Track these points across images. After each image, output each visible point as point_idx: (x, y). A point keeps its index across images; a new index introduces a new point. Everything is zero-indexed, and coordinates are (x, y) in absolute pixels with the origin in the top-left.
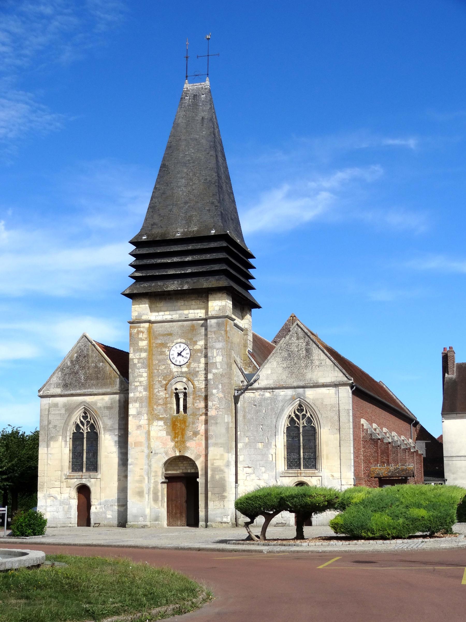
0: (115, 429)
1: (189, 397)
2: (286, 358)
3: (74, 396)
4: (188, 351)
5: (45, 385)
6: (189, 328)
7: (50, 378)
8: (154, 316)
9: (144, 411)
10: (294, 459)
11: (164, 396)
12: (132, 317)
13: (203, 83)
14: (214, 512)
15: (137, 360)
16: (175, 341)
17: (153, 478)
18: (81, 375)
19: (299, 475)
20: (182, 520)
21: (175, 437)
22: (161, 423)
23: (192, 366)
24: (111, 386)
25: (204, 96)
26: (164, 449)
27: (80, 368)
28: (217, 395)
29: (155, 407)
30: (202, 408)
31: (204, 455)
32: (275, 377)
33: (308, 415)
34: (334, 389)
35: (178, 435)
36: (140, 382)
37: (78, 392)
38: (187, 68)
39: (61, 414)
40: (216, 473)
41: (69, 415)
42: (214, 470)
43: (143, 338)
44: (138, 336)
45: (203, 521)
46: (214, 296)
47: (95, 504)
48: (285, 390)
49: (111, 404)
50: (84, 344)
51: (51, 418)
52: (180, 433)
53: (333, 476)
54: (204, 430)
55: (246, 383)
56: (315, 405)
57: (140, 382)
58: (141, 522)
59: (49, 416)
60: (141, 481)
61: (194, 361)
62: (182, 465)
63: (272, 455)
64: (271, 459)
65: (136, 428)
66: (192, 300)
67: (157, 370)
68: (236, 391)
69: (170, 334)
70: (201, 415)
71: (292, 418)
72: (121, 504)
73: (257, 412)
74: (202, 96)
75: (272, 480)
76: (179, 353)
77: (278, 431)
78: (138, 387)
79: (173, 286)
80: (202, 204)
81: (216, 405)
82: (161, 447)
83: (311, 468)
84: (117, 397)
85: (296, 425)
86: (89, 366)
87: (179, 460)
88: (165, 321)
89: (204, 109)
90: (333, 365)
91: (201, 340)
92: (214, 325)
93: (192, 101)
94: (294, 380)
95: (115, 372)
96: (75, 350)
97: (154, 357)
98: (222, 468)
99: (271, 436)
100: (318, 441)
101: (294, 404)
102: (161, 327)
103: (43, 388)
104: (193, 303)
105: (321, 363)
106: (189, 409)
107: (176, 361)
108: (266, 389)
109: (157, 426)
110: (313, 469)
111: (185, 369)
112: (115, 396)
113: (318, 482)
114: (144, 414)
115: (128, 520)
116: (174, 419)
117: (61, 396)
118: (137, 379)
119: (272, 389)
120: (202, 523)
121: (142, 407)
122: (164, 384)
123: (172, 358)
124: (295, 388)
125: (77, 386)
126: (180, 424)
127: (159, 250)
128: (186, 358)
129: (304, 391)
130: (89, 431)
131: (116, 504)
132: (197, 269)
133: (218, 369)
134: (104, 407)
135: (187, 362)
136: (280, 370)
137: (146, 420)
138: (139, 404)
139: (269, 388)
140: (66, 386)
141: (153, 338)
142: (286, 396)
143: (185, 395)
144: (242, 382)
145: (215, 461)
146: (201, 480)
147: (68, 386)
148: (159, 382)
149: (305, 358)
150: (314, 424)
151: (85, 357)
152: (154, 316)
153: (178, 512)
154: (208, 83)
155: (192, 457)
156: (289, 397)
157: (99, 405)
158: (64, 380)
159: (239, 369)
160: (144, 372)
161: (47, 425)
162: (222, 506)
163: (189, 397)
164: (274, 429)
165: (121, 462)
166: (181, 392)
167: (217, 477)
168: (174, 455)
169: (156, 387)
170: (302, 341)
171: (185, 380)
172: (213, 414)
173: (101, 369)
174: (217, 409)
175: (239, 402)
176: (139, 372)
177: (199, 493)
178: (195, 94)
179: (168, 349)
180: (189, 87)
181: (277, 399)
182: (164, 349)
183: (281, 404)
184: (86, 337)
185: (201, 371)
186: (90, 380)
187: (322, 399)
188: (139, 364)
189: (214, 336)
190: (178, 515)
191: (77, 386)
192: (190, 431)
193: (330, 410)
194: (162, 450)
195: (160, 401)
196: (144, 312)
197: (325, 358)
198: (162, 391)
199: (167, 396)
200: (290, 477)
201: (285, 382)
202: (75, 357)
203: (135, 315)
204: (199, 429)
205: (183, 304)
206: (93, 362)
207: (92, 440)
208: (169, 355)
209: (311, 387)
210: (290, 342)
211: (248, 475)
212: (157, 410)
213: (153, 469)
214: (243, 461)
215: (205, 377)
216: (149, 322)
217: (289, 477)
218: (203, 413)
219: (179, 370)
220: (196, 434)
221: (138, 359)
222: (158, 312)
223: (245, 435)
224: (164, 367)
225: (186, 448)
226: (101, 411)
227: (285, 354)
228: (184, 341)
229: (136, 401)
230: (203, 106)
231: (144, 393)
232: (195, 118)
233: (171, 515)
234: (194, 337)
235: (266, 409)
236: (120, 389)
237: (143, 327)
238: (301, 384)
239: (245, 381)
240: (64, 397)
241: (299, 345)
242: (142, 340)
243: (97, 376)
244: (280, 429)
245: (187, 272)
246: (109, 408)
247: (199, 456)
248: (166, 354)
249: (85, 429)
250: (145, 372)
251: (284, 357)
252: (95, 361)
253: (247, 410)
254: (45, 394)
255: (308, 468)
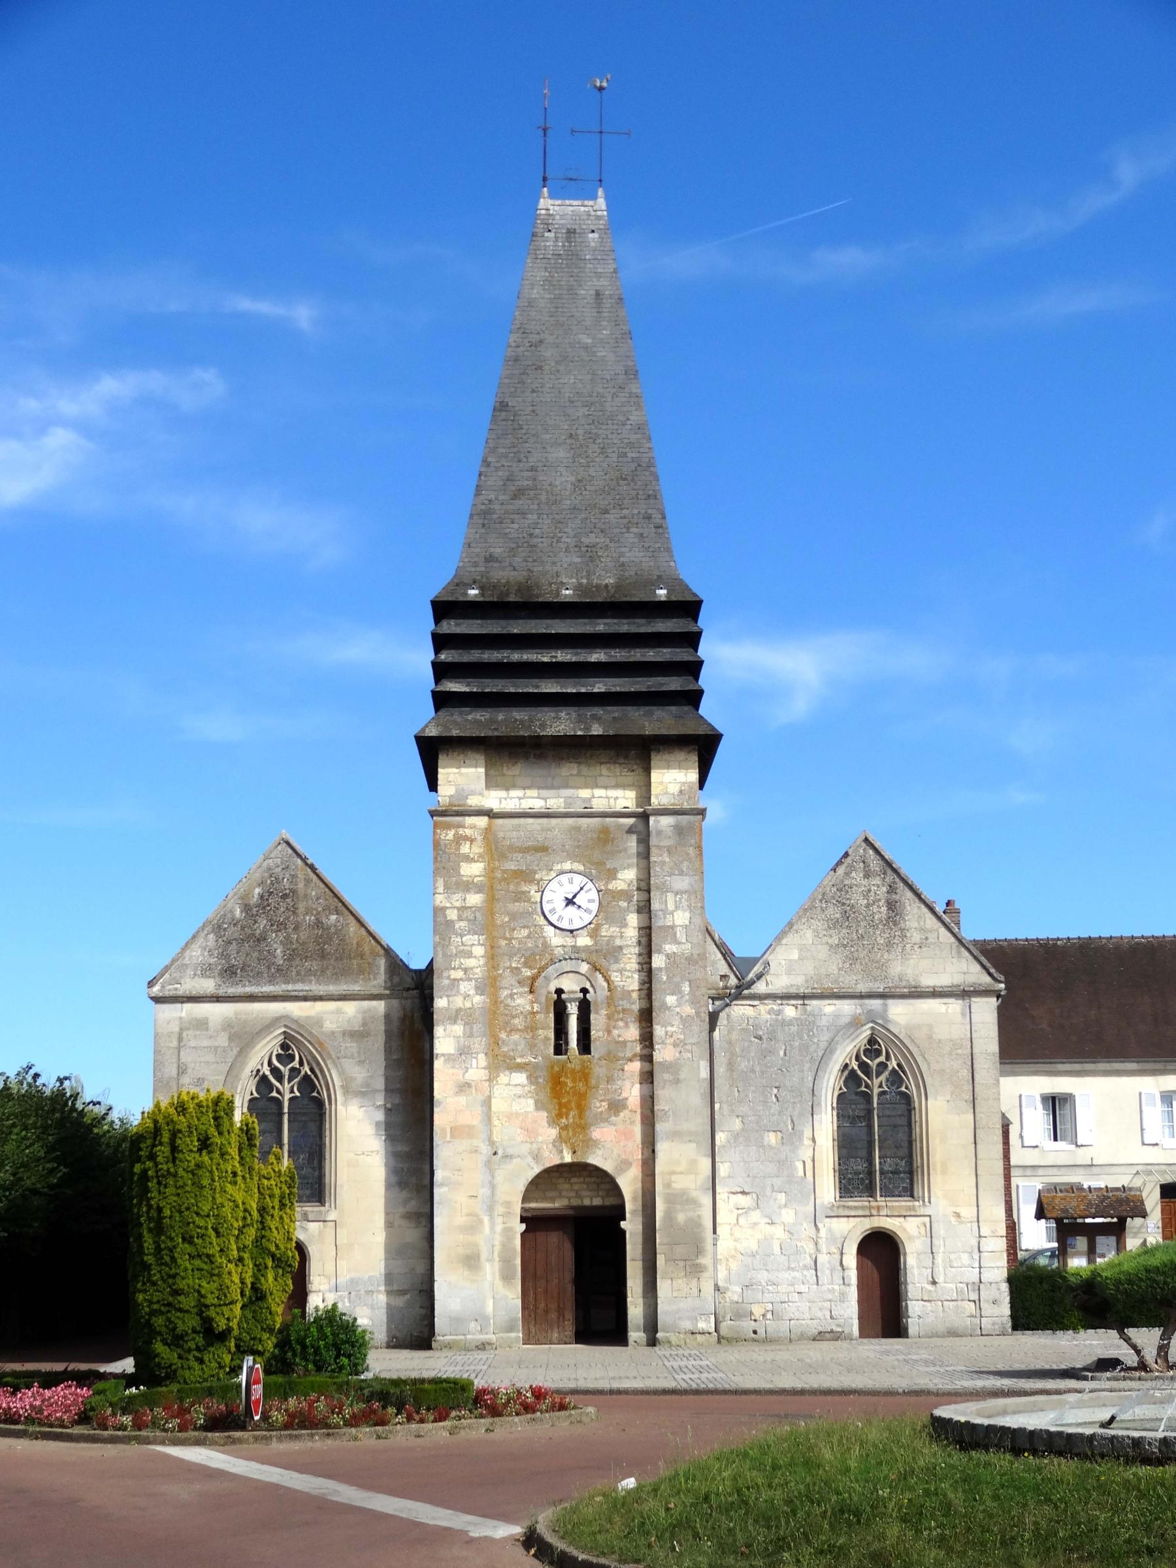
0: (375, 1091)
1: (597, 1013)
2: (837, 921)
3: (253, 1001)
4: (594, 895)
5: (166, 969)
6: (595, 836)
7: (184, 949)
8: (495, 800)
9: (476, 1046)
10: (857, 1173)
11: (528, 1008)
12: (439, 799)
13: (591, 203)
14: (675, 1307)
15: (456, 911)
16: (558, 867)
17: (499, 1220)
18: (275, 946)
19: (874, 1212)
20: (564, 1327)
21: (560, 1116)
22: (520, 1078)
23: (604, 932)
24: (362, 977)
25: (596, 235)
26: (528, 1145)
27: (272, 925)
28: (678, 1010)
29: (503, 1035)
30: (632, 1041)
31: (640, 1163)
32: (809, 968)
33: (893, 1064)
34: (960, 1002)
35: (569, 1110)
36: (466, 970)
37: (267, 989)
38: (545, 157)
39: (216, 1048)
40: (679, 1207)
41: (240, 1052)
42: (671, 1200)
43: (472, 856)
44: (458, 849)
45: (638, 1330)
46: (666, 756)
47: (322, 1288)
48: (834, 1002)
49: (364, 1024)
50: (282, 863)
51: (186, 1057)
52: (573, 1105)
53: (958, 1215)
54: (639, 1098)
55: (733, 981)
56: (913, 1041)
57: (466, 970)
58: (473, 1334)
59: (182, 1053)
60: (473, 1227)
61: (610, 920)
62: (567, 1186)
63: (804, 1162)
64: (801, 1173)
65: (457, 1090)
66: (601, 763)
67: (506, 939)
68: (710, 1001)
69: (543, 849)
70: (631, 1060)
71: (264, 1077)
72: (395, 1287)
73: (764, 1054)
74: (591, 235)
75: (805, 1225)
76: (570, 897)
77: (819, 1104)
78: (461, 982)
79: (561, 723)
80: (618, 516)
81: (675, 1036)
82: (519, 1139)
83: (899, 1196)
84: (380, 1006)
85: (274, 1094)
86: (298, 922)
87: (558, 1174)
88: (529, 813)
89: (599, 270)
90: (957, 943)
91: (629, 866)
92: (669, 831)
93: (564, 246)
94: (860, 977)
95: (373, 941)
96: (257, 876)
97: (498, 906)
98: (694, 1194)
99: (801, 1115)
100: (918, 1130)
101: (857, 1037)
102: (517, 828)
103: (162, 974)
104: (604, 771)
105: (927, 939)
106: (598, 1043)
107: (560, 918)
108: (787, 997)
109: (509, 1084)
110: (906, 1199)
111: (584, 941)
112: (374, 1003)
113: (923, 1230)
114: (477, 1053)
115: (437, 1330)
116: (556, 1069)
117: (217, 999)
118: (457, 962)
119: (804, 997)
120: (636, 1335)
121: (471, 1035)
122: (528, 977)
123: (550, 911)
124: (861, 996)
125: (262, 973)
126: (574, 1081)
127: (517, 627)
128: (587, 911)
129: (885, 1005)
130: (298, 1094)
131: (382, 1288)
132: (619, 686)
133: (680, 943)
134: (344, 1033)
135: (590, 923)
136: (822, 952)
137: (484, 1068)
138: (462, 1027)
139: (796, 997)
140: (229, 973)
141: (496, 857)
142: (837, 1016)
143: (585, 1008)
144: (723, 977)
145: (674, 1178)
146: (631, 1226)
147: (236, 973)
148: (512, 971)
149: (885, 925)
150: (907, 1088)
151: (285, 896)
152: (495, 800)
153: (553, 1306)
154: (601, 203)
155: (608, 1167)
156: (846, 1020)
157: (329, 1026)
158: (224, 955)
159: (716, 944)
160: (476, 943)
161: (175, 1076)
162: (695, 1291)
163: (597, 1013)
164: (808, 1096)
165: (394, 1179)
166: (574, 1000)
167: (681, 1217)
168: (557, 1162)
169: (504, 983)
170: (877, 881)
171: (584, 968)
172: (668, 1059)
173: (333, 930)
174: (678, 1045)
175: (717, 1030)
176: (463, 944)
177: (628, 1258)
178: (569, 227)
179: (536, 888)
180: (551, 207)
181: (814, 1022)
182: (525, 885)
183: (825, 1037)
184: (288, 843)
185: (628, 946)
186: (301, 960)
187: (930, 1027)
188: (463, 924)
189: (667, 860)
190: (553, 1316)
191: (262, 973)
192: (601, 1101)
193: (950, 1054)
194: (525, 1148)
195: (516, 1021)
196: (473, 787)
197: (936, 927)
198: (521, 994)
199: (536, 1007)
200: (851, 1219)
201: (836, 981)
202: (256, 896)
203: (448, 794)
204: (624, 1095)
205: (575, 772)
206: (308, 911)
207: (304, 1118)
208: (541, 902)
209: (903, 996)
210: (846, 882)
211: (740, 1211)
212: (507, 1045)
213: (501, 1196)
214: (729, 1177)
215: (639, 963)
216: (490, 814)
217: (848, 1217)
218: (635, 1055)
219: (569, 941)
220: (617, 1106)
221: (459, 909)
222: (507, 789)
223: (733, 1111)
224: (525, 932)
225: (591, 1143)
226: (335, 1044)
227: (834, 912)
228: (582, 868)
229: (454, 1019)
230: (596, 262)
231: (478, 999)
232: (578, 292)
233: (533, 1316)
234: (607, 859)
235: (788, 1048)
236: (389, 984)
237: (473, 827)
238: (880, 987)
239: (732, 976)
240: (231, 1002)
241: (869, 891)
242: (468, 859)
243: (323, 950)
244: (823, 1098)
245: (596, 690)
246: (358, 1035)
247: (625, 1164)
248: (532, 900)
249: (287, 1091)
250: (479, 944)
251: (832, 920)
252: (316, 909)
253: (737, 1049)
254: (167, 994)
255: (893, 1196)
